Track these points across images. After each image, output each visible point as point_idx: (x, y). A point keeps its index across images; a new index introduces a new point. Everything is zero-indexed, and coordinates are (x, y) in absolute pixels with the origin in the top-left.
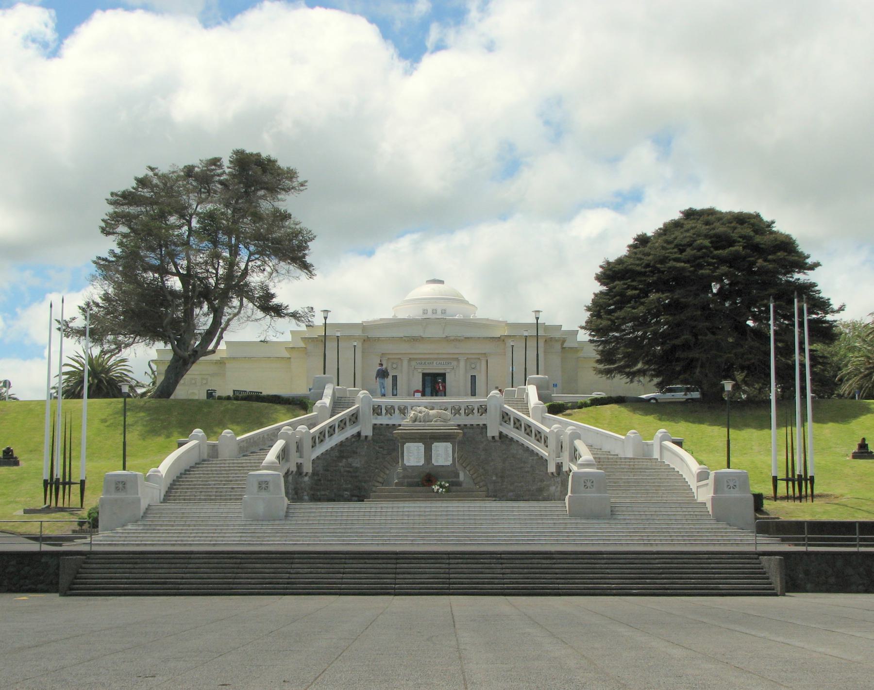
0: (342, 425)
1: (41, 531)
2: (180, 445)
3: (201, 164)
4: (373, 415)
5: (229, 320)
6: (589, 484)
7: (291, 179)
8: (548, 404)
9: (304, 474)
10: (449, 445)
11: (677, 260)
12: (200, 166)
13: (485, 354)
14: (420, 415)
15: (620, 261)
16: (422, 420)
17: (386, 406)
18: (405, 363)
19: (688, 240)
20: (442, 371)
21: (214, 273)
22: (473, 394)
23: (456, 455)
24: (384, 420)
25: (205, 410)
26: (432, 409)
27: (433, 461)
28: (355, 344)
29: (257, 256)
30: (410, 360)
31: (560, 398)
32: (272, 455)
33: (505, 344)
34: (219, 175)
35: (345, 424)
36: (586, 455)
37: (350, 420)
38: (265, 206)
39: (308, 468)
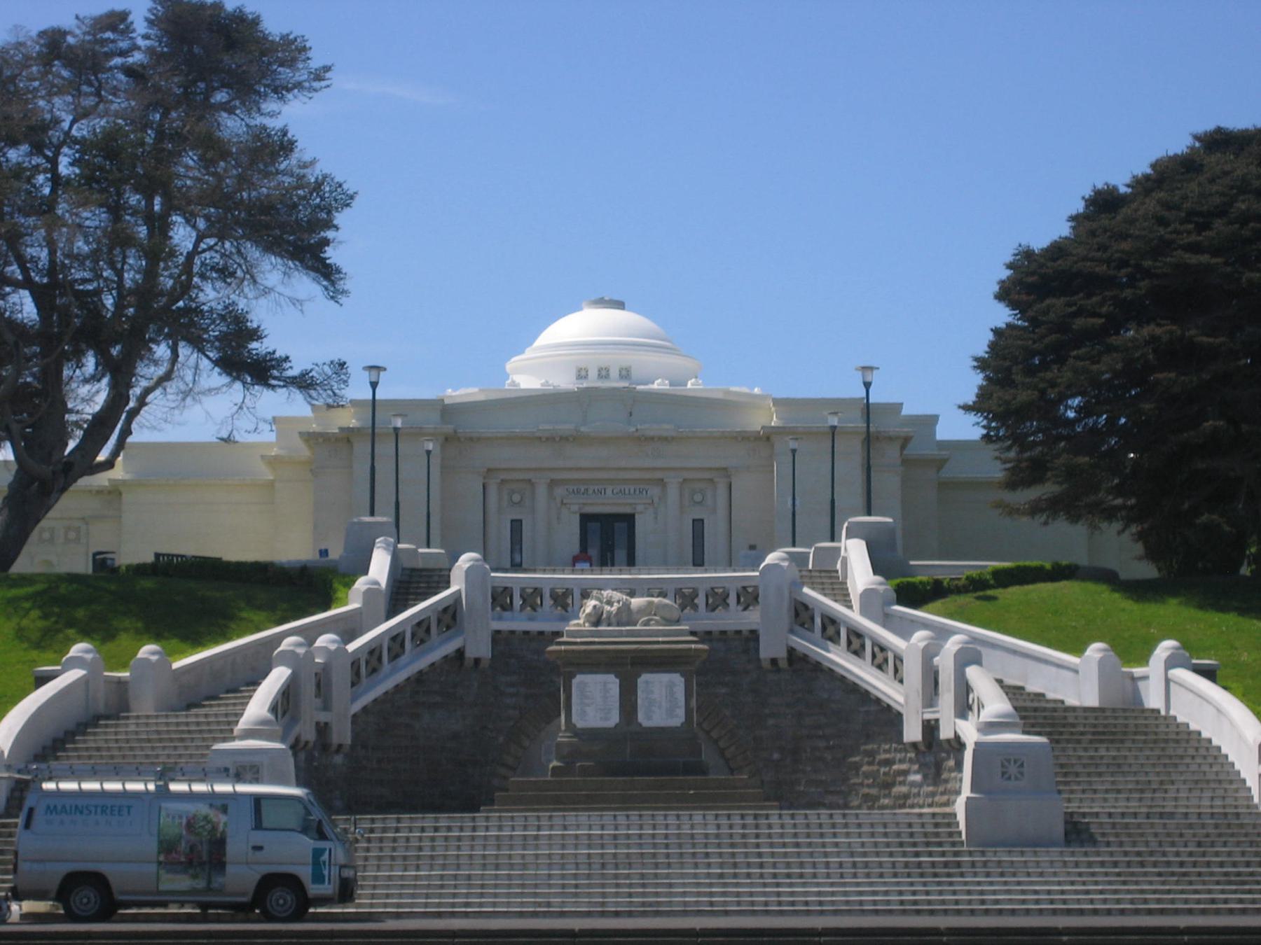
0: (421, 633)
1: (158, 887)
2: (42, 680)
3: (79, 27)
4: (493, 609)
5: (148, 391)
6: (1013, 769)
7: (291, 63)
8: (898, 581)
9: (334, 748)
10: (677, 680)
11: (1194, 248)
12: (78, 32)
13: (725, 469)
14: (607, 608)
15: (1057, 250)
16: (613, 620)
17: (523, 590)
18: (542, 491)
19: (1217, 200)
20: (628, 510)
21: (113, 281)
22: (698, 561)
23: (694, 703)
24: (517, 623)
25: (1240, 506)
26: (632, 594)
27: (641, 717)
28: (430, 446)
29: (211, 241)
30: (553, 484)
31: (928, 567)
32: (259, 704)
33: (772, 446)
34: (123, 53)
35: (428, 630)
36: (995, 705)
37: (439, 621)
38: (233, 126)
39: (342, 734)
